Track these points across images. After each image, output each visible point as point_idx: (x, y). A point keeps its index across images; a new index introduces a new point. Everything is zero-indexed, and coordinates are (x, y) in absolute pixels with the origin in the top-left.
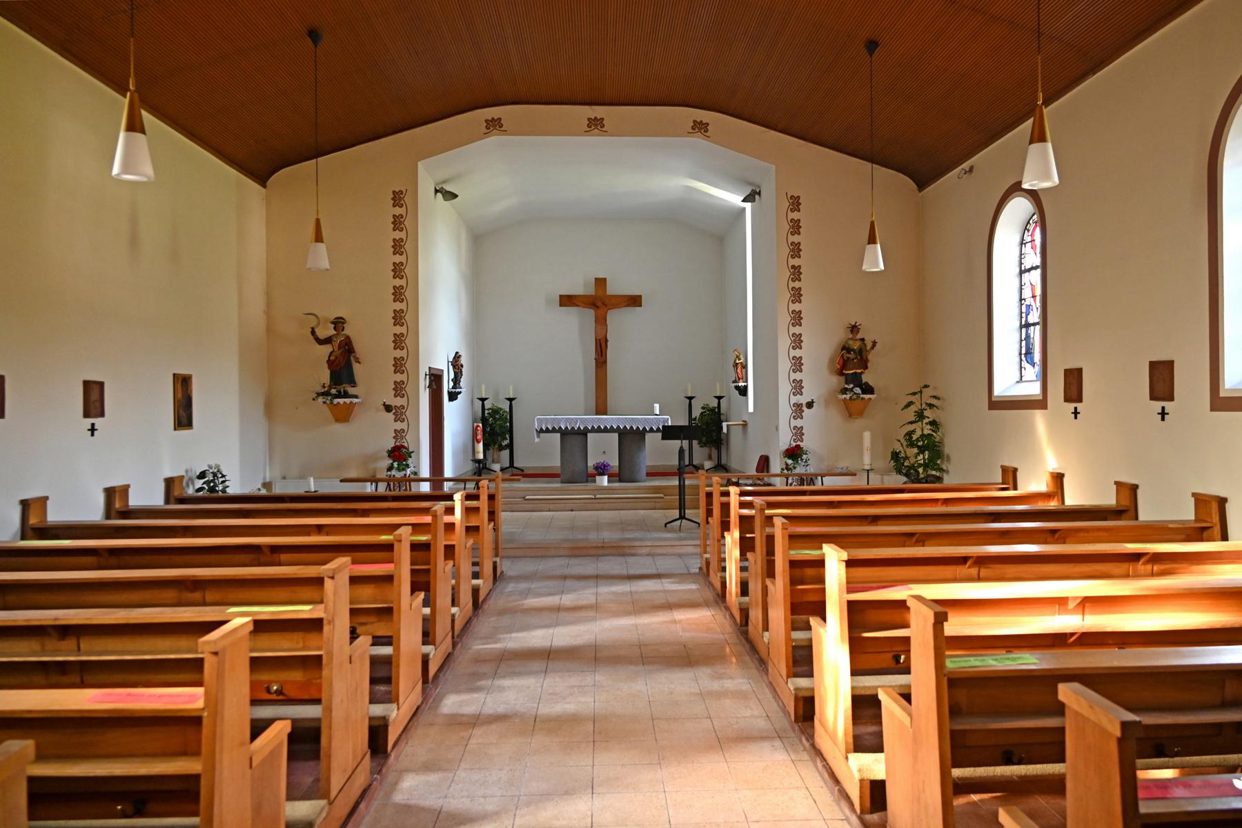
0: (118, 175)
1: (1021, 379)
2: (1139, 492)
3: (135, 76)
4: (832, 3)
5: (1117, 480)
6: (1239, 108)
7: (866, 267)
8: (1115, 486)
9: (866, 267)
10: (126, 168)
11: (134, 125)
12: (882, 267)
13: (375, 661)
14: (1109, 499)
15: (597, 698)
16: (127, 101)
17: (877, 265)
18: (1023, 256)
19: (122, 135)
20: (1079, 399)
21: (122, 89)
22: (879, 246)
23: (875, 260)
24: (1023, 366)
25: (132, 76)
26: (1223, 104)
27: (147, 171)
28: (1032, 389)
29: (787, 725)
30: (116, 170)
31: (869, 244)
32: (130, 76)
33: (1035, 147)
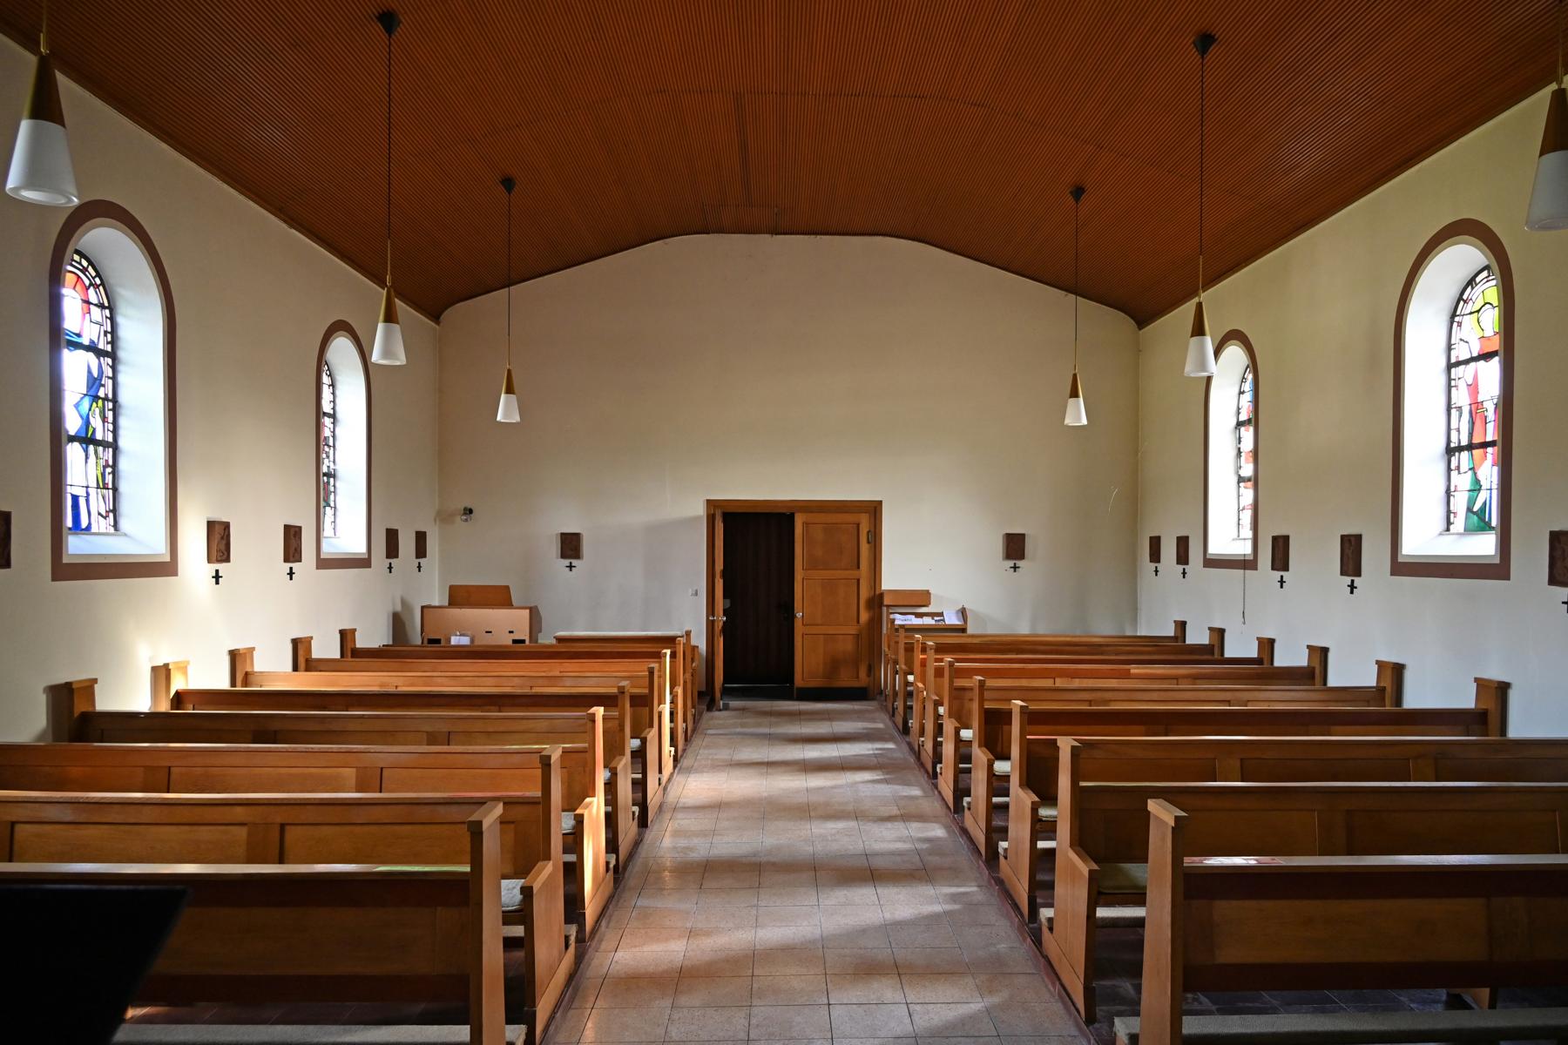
0: (16, 189)
1: (1448, 530)
2: (1276, 646)
3: (391, 273)
4: (1085, 4)
5: (1479, 676)
6: (1438, 253)
7: (1069, 421)
8: (1307, 650)
9: (1069, 421)
10: (33, 177)
11: (45, 107)
12: (1084, 421)
13: (566, 865)
14: (1466, 700)
15: (809, 832)
16: (385, 292)
17: (1079, 419)
18: (1457, 319)
19: (381, 327)
20: (1187, 563)
21: (382, 284)
22: (1081, 399)
23: (1077, 414)
24: (1452, 508)
25: (44, 30)
26: (1423, 244)
27: (401, 359)
28: (1245, 549)
29: (1074, 1031)
30: (11, 183)
31: (1071, 397)
32: (387, 274)
33: (1072, 401)
